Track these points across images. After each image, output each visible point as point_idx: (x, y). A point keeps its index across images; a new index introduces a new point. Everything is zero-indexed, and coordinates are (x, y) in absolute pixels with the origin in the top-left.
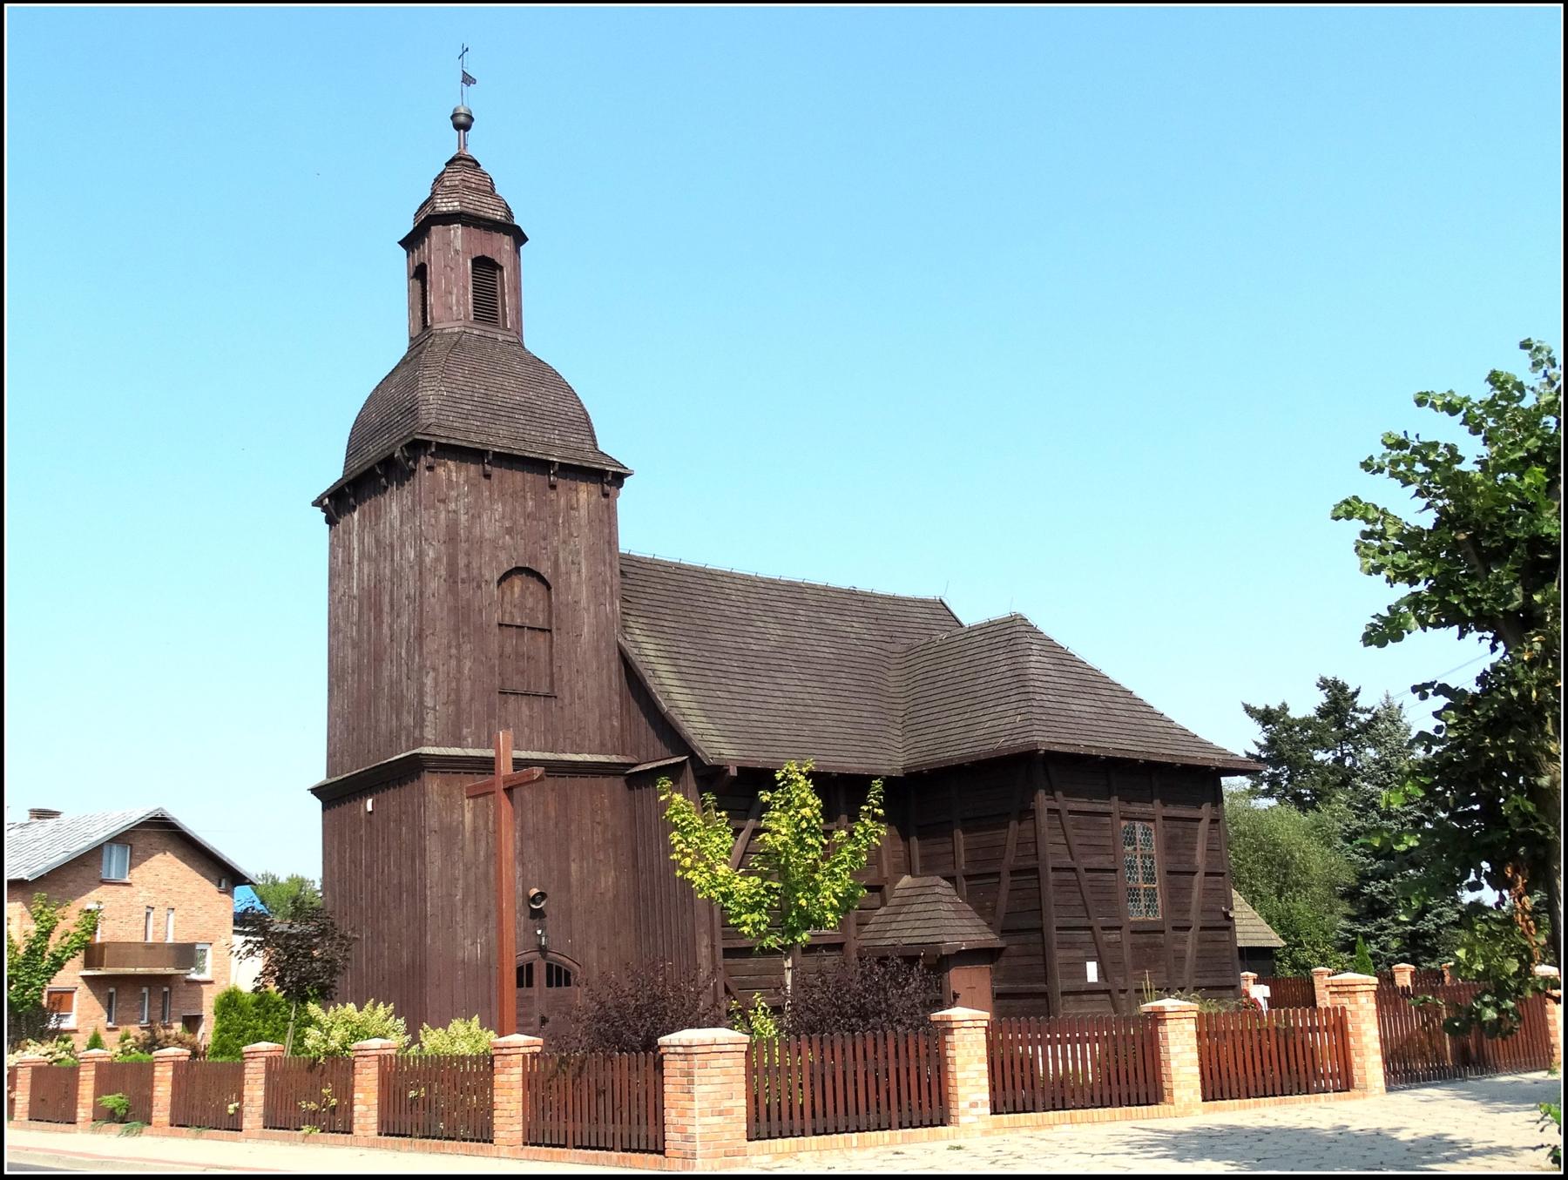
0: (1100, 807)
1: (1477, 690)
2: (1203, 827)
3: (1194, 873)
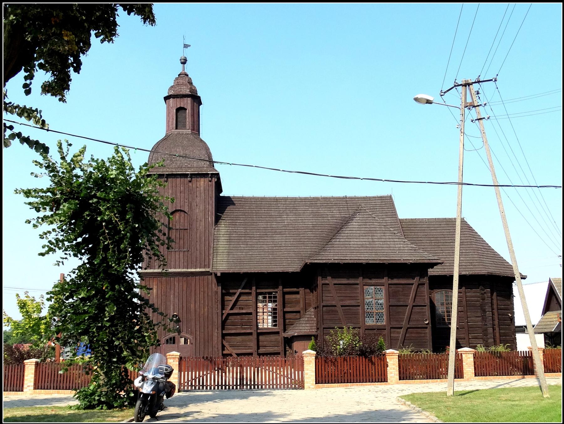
0: (352, 281)
1: (85, 258)
2: (414, 287)
3: (407, 306)
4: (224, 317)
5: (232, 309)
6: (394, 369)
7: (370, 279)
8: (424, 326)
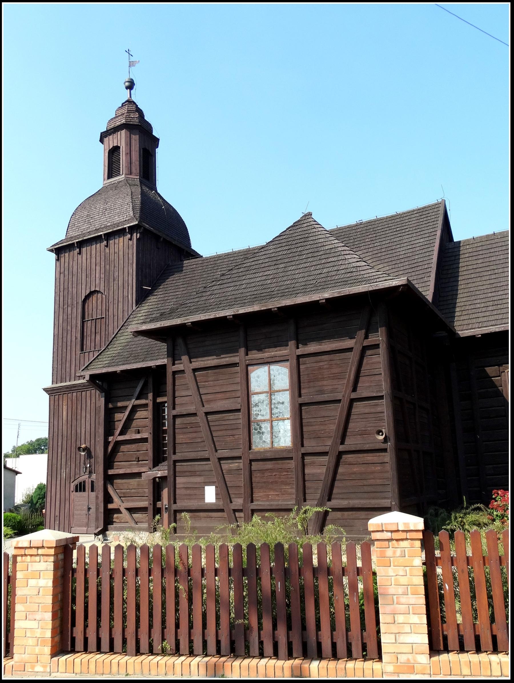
0: (226, 359)
2: (353, 357)
4: (110, 448)
7: (260, 349)
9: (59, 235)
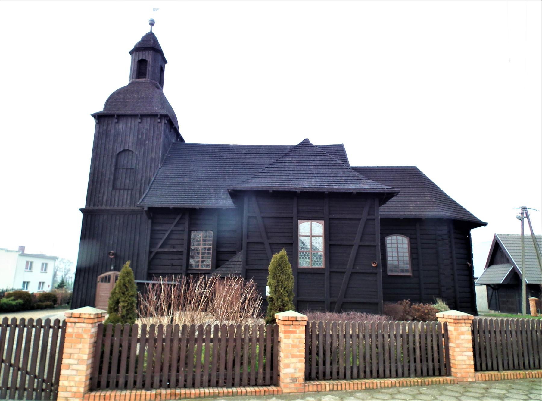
2: (362, 224)
4: (152, 256)
5: (161, 247)
6: (294, 356)
8: (371, 271)
9: (100, 108)
